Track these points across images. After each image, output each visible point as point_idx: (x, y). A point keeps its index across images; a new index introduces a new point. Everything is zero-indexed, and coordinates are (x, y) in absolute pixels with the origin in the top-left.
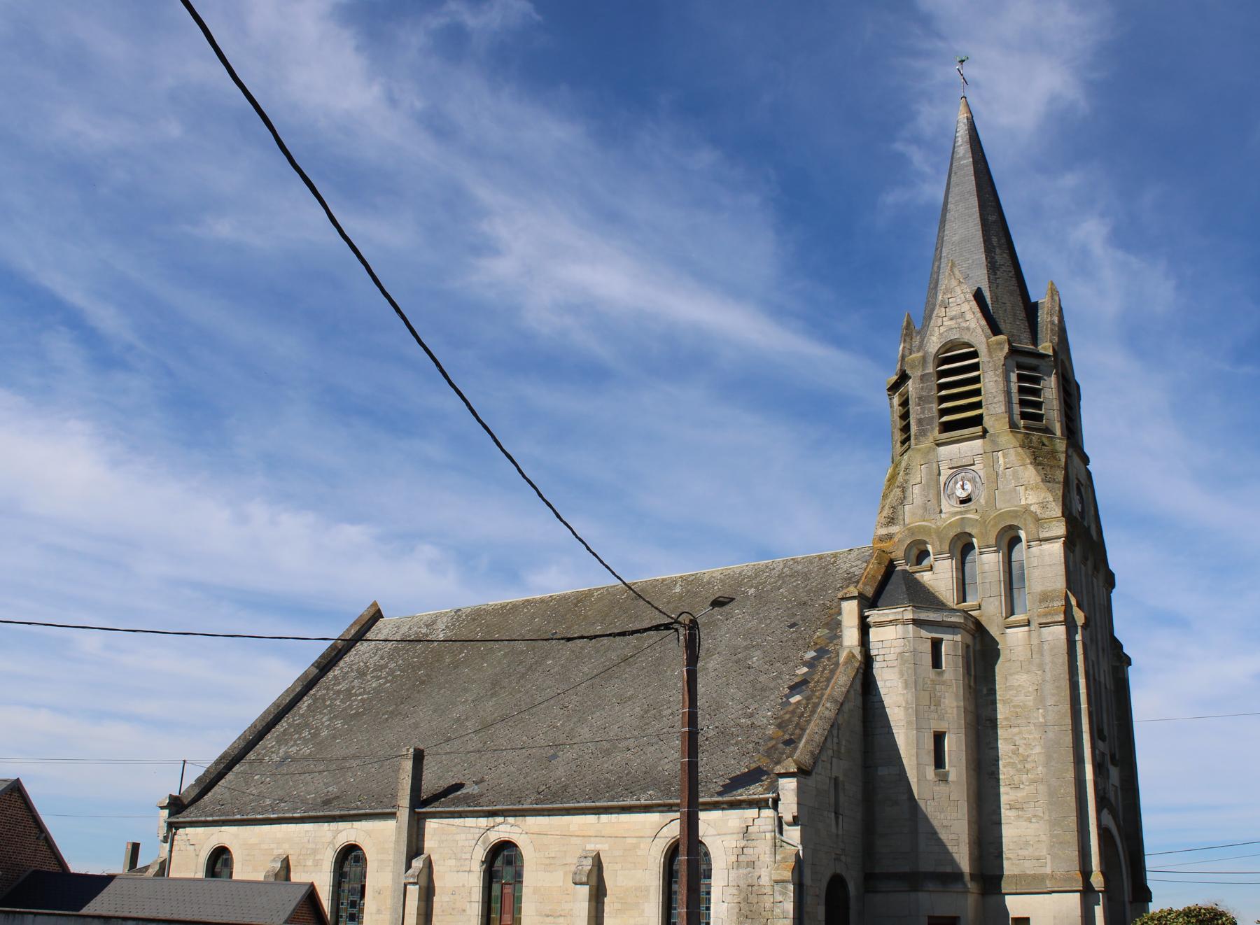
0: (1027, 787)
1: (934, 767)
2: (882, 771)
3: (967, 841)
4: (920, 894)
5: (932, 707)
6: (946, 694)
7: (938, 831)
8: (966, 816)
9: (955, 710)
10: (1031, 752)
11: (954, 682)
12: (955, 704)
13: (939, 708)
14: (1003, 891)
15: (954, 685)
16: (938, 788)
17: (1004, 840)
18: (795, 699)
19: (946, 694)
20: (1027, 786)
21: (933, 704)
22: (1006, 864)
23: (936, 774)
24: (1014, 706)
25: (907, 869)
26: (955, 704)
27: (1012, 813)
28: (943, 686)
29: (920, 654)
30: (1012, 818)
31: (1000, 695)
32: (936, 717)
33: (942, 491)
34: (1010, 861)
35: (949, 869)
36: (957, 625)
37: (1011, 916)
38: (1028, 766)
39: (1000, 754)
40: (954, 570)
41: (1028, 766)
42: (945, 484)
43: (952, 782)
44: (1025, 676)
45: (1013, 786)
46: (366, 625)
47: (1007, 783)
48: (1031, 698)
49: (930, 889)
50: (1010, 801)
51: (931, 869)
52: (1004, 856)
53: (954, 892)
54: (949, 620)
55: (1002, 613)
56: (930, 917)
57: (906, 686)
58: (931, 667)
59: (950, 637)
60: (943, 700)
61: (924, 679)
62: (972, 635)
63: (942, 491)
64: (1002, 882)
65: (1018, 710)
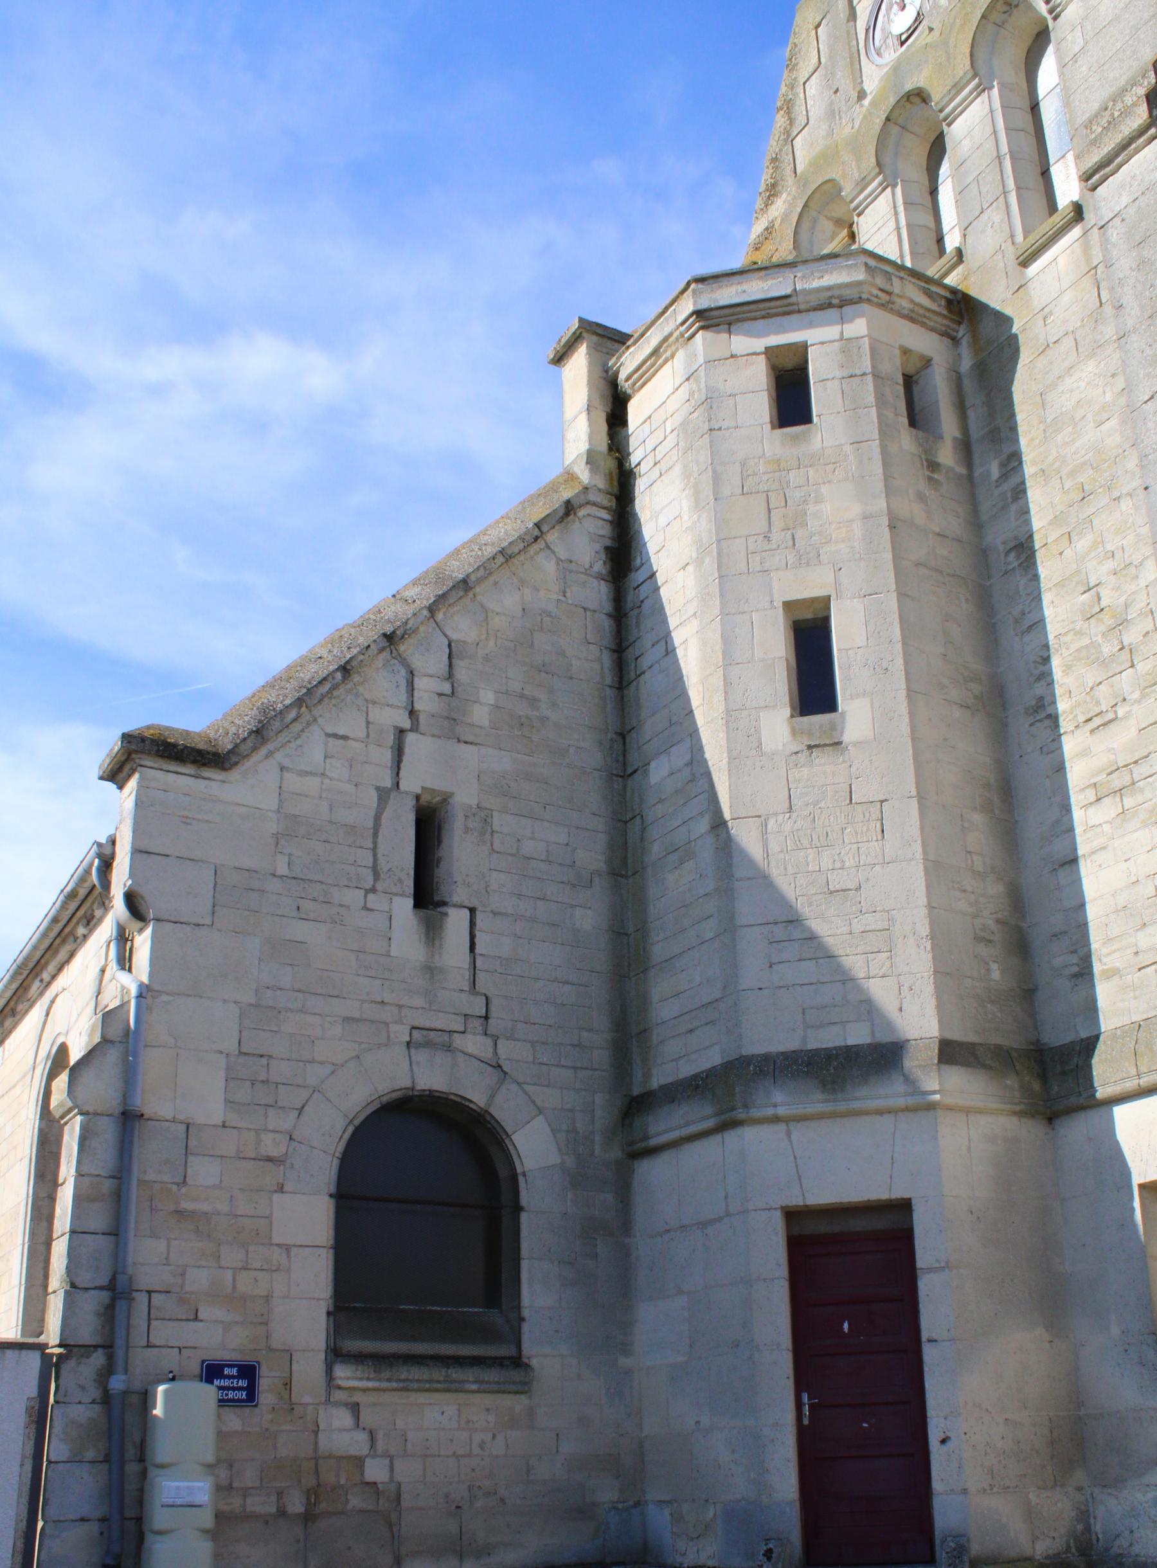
0: (1135, 708)
1: (787, 711)
2: (659, 772)
3: (924, 929)
4: (749, 1134)
5: (776, 536)
6: (824, 489)
7: (803, 908)
8: (918, 847)
9: (857, 529)
10: (1133, 588)
11: (848, 449)
12: (856, 510)
13: (800, 534)
14: (1101, 1093)
15: (851, 458)
16: (805, 772)
17: (1093, 912)
18: (574, 725)
19: (824, 489)
20: (1138, 702)
21: (777, 524)
22: (1104, 992)
23: (794, 732)
24: (1072, 474)
25: (713, 1059)
26: (856, 510)
27: (1108, 809)
28: (811, 472)
29: (731, 401)
30: (1106, 827)
31: (1034, 463)
32: (791, 559)
33: (862, 51)
34: (1116, 979)
35: (857, 1036)
36: (848, 293)
37: (1137, 1179)
38: (1131, 636)
39: (1051, 637)
40: (901, 209)
41: (1131, 636)
42: (867, 30)
43: (856, 744)
44: (1089, 368)
45: (1097, 721)
46: (399, 1093)
47: (1081, 719)
48: (1113, 422)
49: (782, 1111)
50: (1093, 776)
51: (791, 1044)
52: (1097, 968)
53: (880, 1112)
54: (816, 284)
55: (1012, 236)
56: (792, 1215)
57: (697, 506)
58: (769, 426)
59: (830, 332)
60: (812, 509)
61: (743, 465)
62: (944, 334)
63: (862, 51)
64: (1095, 1061)
65: (1082, 478)
